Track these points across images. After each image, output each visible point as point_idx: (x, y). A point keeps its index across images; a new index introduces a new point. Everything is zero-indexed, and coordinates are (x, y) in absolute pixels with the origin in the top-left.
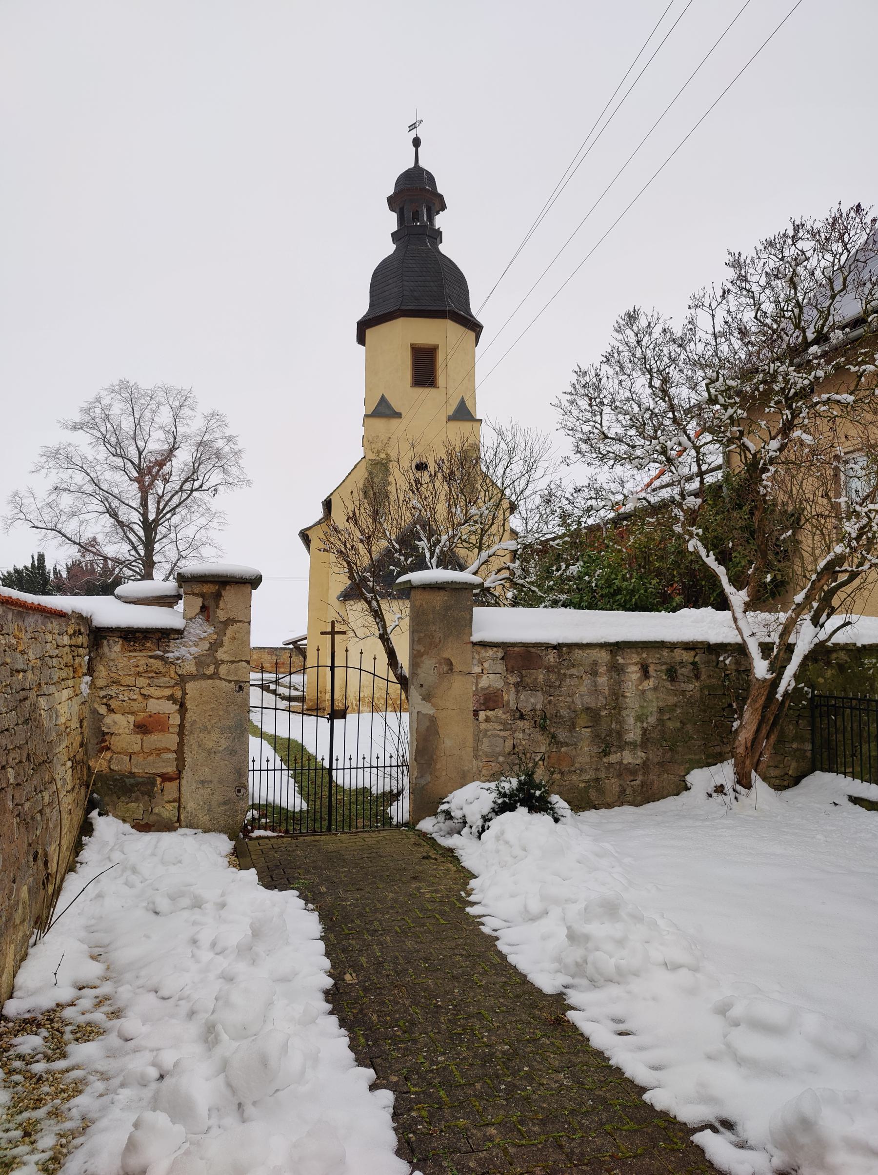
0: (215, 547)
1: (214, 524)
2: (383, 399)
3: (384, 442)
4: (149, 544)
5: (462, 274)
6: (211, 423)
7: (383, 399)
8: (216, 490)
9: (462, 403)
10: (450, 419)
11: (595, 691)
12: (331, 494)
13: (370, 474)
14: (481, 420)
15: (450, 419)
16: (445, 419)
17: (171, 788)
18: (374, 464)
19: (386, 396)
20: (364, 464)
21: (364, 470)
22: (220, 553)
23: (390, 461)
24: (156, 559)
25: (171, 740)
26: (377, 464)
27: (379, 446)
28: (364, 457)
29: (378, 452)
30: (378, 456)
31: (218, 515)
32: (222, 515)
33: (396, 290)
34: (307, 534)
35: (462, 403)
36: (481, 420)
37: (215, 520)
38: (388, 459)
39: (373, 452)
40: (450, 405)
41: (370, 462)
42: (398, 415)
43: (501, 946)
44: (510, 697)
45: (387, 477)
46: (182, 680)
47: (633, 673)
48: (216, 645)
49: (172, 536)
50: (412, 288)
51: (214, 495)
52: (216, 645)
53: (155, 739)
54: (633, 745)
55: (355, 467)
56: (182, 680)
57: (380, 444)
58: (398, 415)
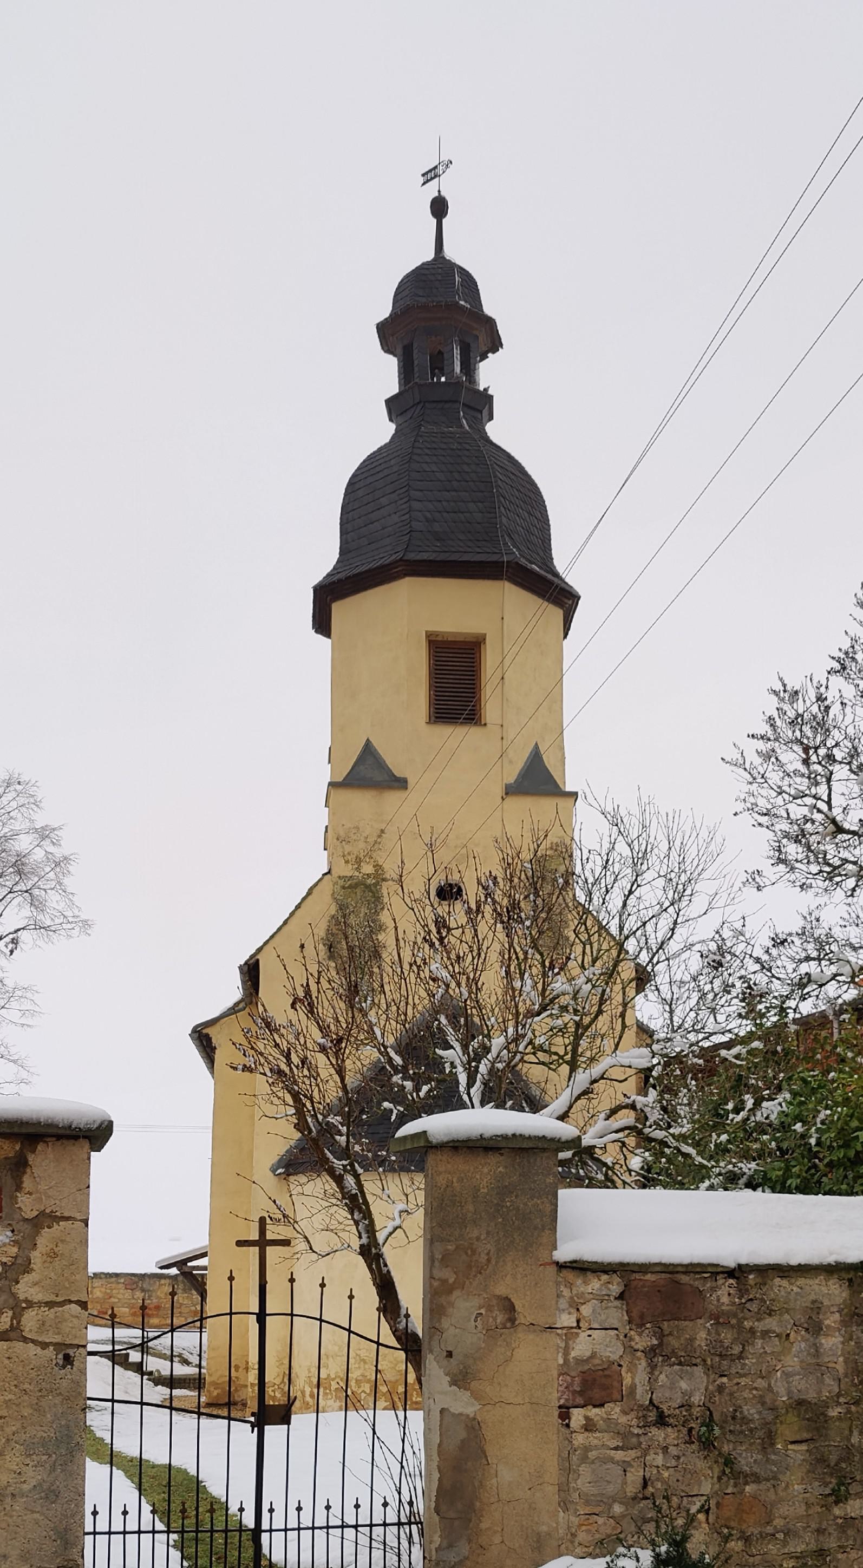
0: (15, 1062)
2: (368, 750)
3: (371, 840)
7: (368, 750)
8: (15, 942)
9: (536, 758)
10: (510, 791)
12: (259, 950)
13: (342, 907)
15: (510, 791)
16: (499, 791)
18: (350, 887)
19: (375, 743)
20: (327, 886)
21: (328, 898)
22: (24, 1074)
23: (384, 880)
27: (359, 847)
28: (329, 872)
29: (359, 861)
30: (358, 869)
32: (29, 995)
33: (395, 518)
34: (207, 1035)
35: (536, 758)
36: (576, 794)
37: (14, 1004)
38: (379, 876)
39: (347, 862)
40: (511, 762)
41: (341, 882)
42: (401, 784)
50: (428, 515)
51: (12, 952)
57: (362, 845)
58: (401, 784)
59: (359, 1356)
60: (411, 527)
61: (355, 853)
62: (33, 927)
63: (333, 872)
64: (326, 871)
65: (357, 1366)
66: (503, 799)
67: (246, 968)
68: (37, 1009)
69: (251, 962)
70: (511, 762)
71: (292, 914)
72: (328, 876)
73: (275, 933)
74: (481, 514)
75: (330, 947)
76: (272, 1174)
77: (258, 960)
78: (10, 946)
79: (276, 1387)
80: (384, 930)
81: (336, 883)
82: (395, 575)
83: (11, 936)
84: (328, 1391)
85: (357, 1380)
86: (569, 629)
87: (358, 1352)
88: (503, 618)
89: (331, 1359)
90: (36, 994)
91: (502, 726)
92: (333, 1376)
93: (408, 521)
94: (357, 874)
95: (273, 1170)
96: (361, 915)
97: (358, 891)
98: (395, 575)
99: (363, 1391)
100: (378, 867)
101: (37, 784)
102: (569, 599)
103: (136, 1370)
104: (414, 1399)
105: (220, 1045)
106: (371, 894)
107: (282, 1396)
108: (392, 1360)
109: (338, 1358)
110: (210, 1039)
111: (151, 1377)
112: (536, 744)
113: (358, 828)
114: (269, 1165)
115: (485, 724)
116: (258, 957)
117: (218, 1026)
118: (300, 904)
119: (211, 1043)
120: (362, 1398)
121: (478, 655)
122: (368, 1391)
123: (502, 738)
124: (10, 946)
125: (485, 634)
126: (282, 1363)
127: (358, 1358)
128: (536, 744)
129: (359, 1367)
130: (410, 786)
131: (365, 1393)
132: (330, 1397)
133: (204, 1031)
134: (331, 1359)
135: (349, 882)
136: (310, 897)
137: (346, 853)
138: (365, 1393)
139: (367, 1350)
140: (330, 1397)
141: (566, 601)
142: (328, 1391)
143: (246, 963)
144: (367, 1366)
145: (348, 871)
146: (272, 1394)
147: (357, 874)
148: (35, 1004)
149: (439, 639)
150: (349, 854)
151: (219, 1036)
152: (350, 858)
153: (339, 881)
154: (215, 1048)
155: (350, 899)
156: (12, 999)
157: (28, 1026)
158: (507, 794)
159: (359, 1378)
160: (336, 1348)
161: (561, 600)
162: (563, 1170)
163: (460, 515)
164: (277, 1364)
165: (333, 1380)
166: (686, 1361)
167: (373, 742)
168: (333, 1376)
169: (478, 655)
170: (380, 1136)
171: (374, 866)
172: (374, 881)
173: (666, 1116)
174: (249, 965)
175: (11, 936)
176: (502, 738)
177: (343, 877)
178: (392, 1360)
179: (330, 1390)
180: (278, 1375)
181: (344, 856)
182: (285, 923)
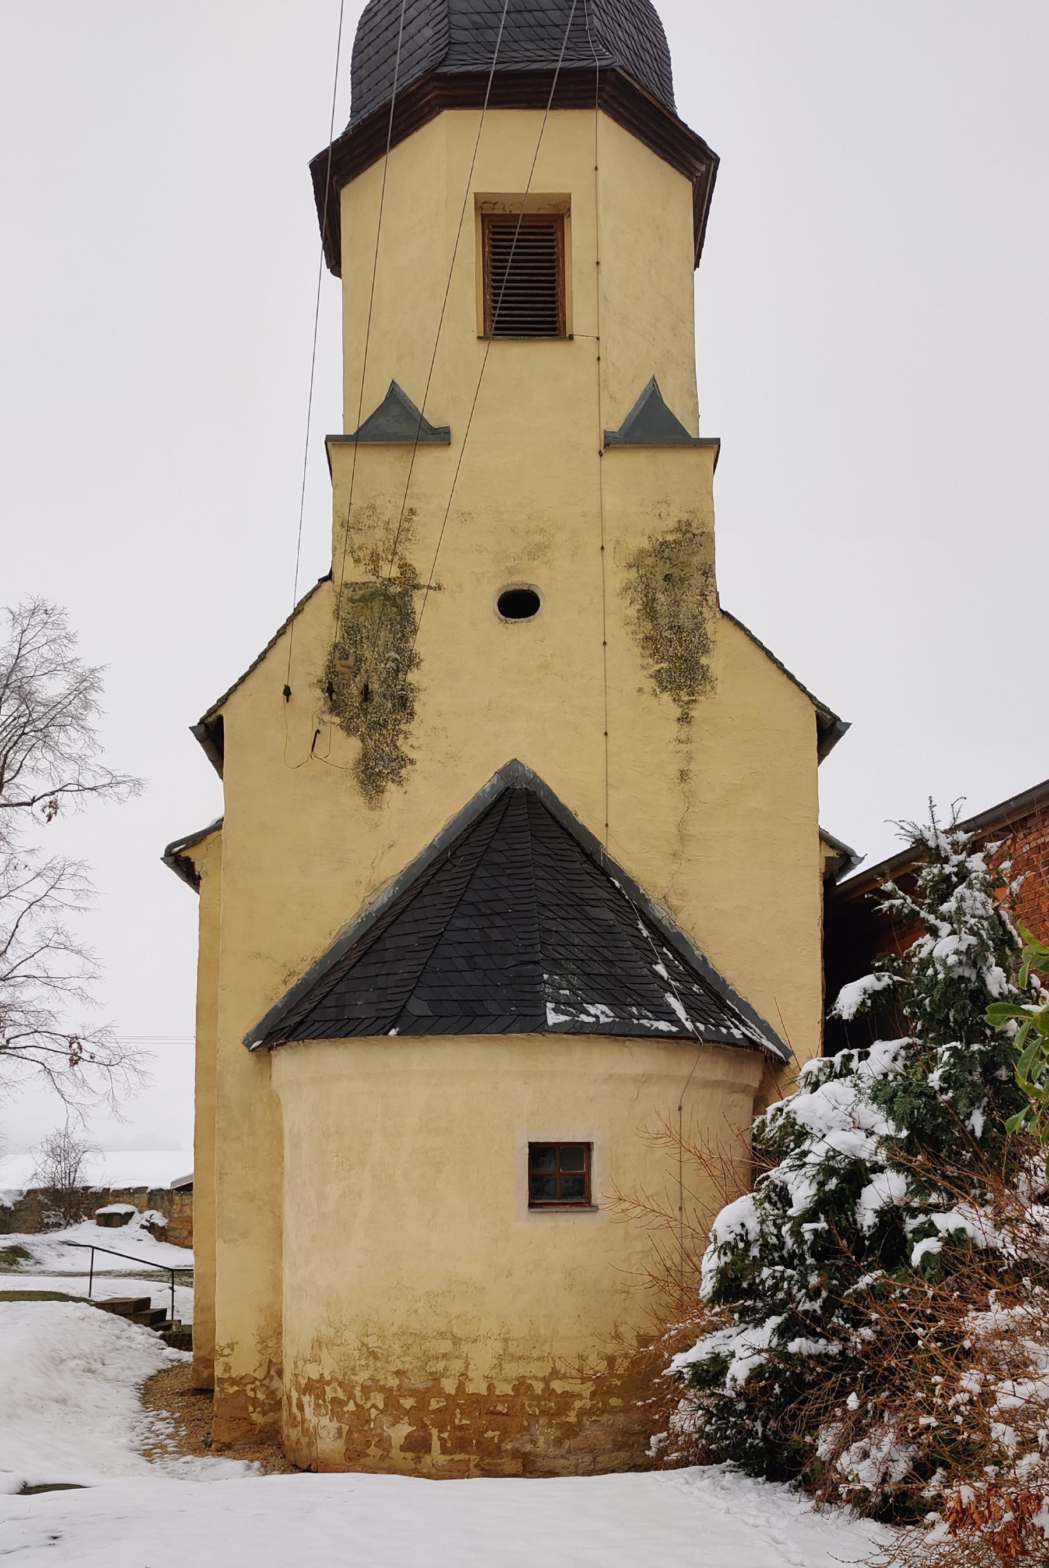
0: (79, 952)
1: (65, 896)
2: (394, 395)
3: (394, 526)
5: (666, 52)
6: (29, 635)
7: (394, 395)
8: (54, 805)
9: (652, 400)
10: (610, 443)
12: (223, 701)
13: (351, 631)
14: (717, 442)
15: (610, 443)
16: (594, 442)
18: (363, 599)
19: (403, 386)
20: (327, 598)
21: (327, 617)
22: (90, 967)
23: (417, 587)
26: (373, 596)
27: (376, 538)
28: (329, 578)
29: (375, 559)
30: (375, 571)
31: (70, 870)
32: (81, 873)
33: (428, 32)
34: (188, 859)
35: (652, 400)
36: (717, 442)
37: (64, 883)
38: (409, 582)
39: (357, 561)
40: (612, 398)
41: (348, 593)
42: (442, 437)
43: (778, 1484)
45: (404, 638)
50: (477, 18)
51: (50, 817)
55: (298, 611)
57: (380, 533)
58: (442, 437)
59: (367, 1345)
60: (450, 37)
61: (370, 546)
62: (76, 787)
63: (336, 577)
64: (327, 573)
65: (363, 1362)
66: (601, 454)
67: (202, 728)
68: (92, 889)
69: (210, 719)
70: (612, 398)
71: (273, 643)
72: (329, 583)
73: (248, 674)
74: (559, 12)
75: (330, 690)
76: (243, 1049)
77: (220, 719)
78: (48, 810)
79: (258, 1383)
80: (417, 665)
81: (340, 595)
82: (426, 109)
83: (47, 799)
84: (321, 1402)
85: (363, 1387)
86: (701, 245)
87: (365, 1340)
88: (596, 168)
89: (324, 1349)
90: (88, 871)
91: (598, 339)
92: (328, 1378)
93: (447, 28)
94: (373, 579)
95: (247, 1043)
96: (380, 643)
97: (376, 606)
98: (426, 109)
99: (374, 1406)
100: (404, 567)
101: (65, 611)
102: (702, 163)
103: (149, 1323)
104: (457, 1421)
105: (206, 874)
106: (395, 609)
107: (267, 1398)
108: (420, 1354)
109: (335, 1348)
110: (193, 864)
111: (167, 1333)
112: (654, 379)
113: (373, 507)
114: (242, 1035)
115: (571, 337)
116: (221, 712)
117: (203, 846)
118: (285, 627)
119: (194, 870)
120: (373, 1417)
121: (560, 235)
122: (381, 1406)
123: (599, 359)
124: (48, 810)
125: (570, 195)
126: (267, 1346)
127: (365, 1349)
128: (654, 379)
129: (367, 1365)
130: (457, 434)
131: (377, 1408)
132: (323, 1411)
133: (183, 854)
134: (324, 1349)
135: (361, 592)
136: (300, 617)
137: (355, 547)
138: (377, 1408)
139: (379, 1336)
140: (323, 1411)
141: (697, 164)
142: (321, 1402)
143: (202, 722)
144: (379, 1365)
145: (357, 574)
146: (251, 1394)
147: (373, 579)
148: (89, 882)
149: (498, 211)
150: (360, 548)
151: (204, 861)
152: (361, 555)
153: (346, 591)
154: (200, 878)
155: (362, 619)
156: (62, 877)
157: (85, 909)
158: (607, 445)
159: (365, 1383)
160: (332, 1331)
161: (689, 163)
162: (707, 1028)
163: (526, 15)
164: (259, 1347)
165: (329, 1383)
167: (400, 385)
168: (328, 1378)
169: (560, 235)
170: (398, 977)
171: (400, 567)
172: (399, 589)
173: (909, 900)
174: (206, 726)
175: (47, 799)
176: (599, 359)
177: (351, 584)
178: (420, 1354)
179: (324, 1401)
180: (261, 1365)
181: (352, 552)
182: (262, 657)
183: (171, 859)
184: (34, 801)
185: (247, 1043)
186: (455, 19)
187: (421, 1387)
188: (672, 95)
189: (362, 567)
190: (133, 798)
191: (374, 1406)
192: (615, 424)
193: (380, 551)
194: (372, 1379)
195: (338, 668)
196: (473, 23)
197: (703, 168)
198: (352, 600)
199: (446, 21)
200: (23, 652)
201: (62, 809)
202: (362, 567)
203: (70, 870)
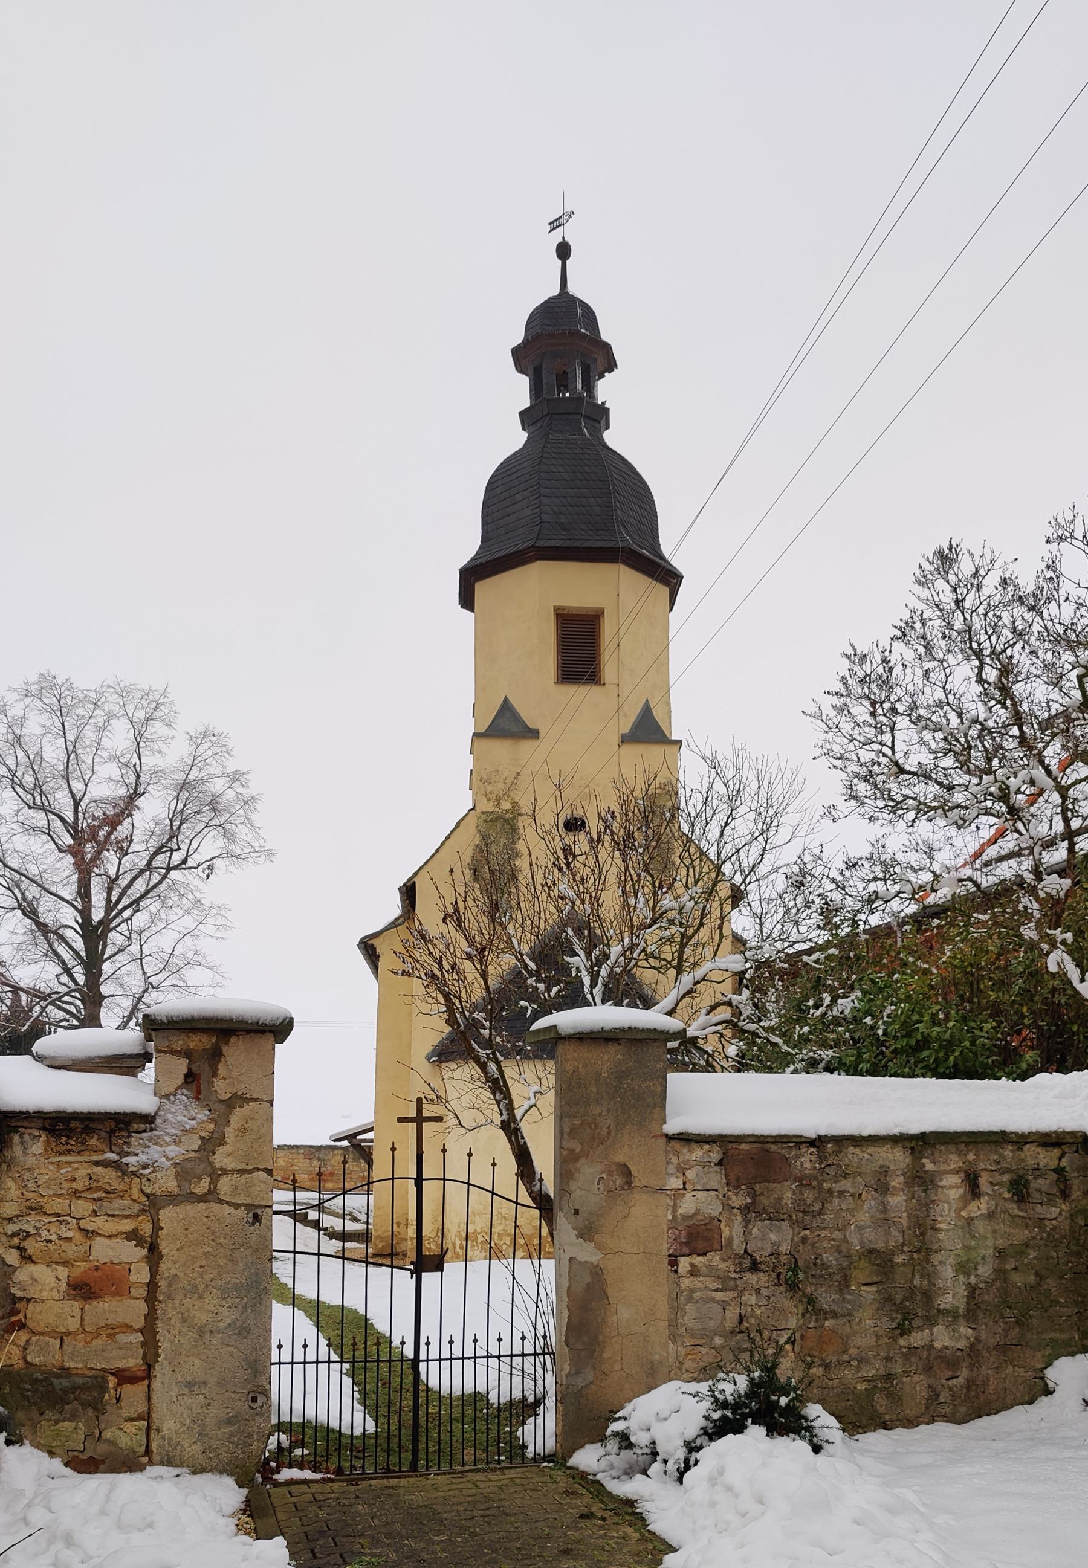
0: (210, 968)
1: (208, 929)
2: (506, 706)
3: (509, 781)
4: (93, 963)
6: (201, 749)
8: (210, 868)
9: (647, 711)
10: (625, 739)
11: (884, 1219)
12: (416, 874)
14: (680, 742)
15: (625, 739)
16: (616, 739)
17: (133, 1393)
18: (491, 821)
19: (511, 699)
20: (472, 820)
21: (473, 830)
22: (219, 979)
23: (520, 815)
24: (105, 989)
25: (135, 1310)
27: (499, 788)
28: (474, 809)
29: (498, 799)
30: (498, 806)
32: (222, 912)
33: (528, 512)
34: (372, 945)
35: (647, 711)
37: (210, 920)
39: (489, 800)
40: (626, 715)
41: (484, 817)
44: (733, 1231)
46: (153, 1204)
47: (952, 1187)
48: (211, 1143)
49: (134, 948)
50: (555, 508)
51: (208, 877)
52: (211, 1143)
53: (105, 1309)
54: (952, 1315)
56: (153, 1204)
57: (501, 785)
67: (405, 888)
68: (229, 924)
70: (626, 715)
71: (443, 844)
72: (473, 811)
77: (414, 883)
78: (207, 872)
83: (207, 863)
85: (499, 1234)
87: (500, 1211)
95: (428, 1058)
97: (499, 824)
100: (514, 804)
105: (383, 954)
110: (375, 949)
116: (414, 880)
118: (449, 835)
124: (207, 872)
133: (370, 942)
136: (458, 829)
143: (404, 885)
144: (507, 1222)
145: (489, 807)
147: (497, 810)
150: (490, 793)
158: (622, 742)
160: (482, 1207)
165: (479, 1234)
166: (775, 1216)
175: (207, 863)
181: (486, 795)
182: (437, 851)
183: (363, 946)
184: (199, 866)
185: (428, 1058)
186: (542, 490)
187: (529, 1233)
188: (658, 537)
189: (491, 803)
190: (268, 863)
191: (504, 1243)
192: (626, 730)
193: (501, 795)
194: (504, 1230)
195: (478, 858)
196: (553, 510)
197: (675, 581)
198: (486, 821)
199: (538, 509)
200: (196, 762)
201: (215, 870)
202: (491, 803)
203: (214, 911)
